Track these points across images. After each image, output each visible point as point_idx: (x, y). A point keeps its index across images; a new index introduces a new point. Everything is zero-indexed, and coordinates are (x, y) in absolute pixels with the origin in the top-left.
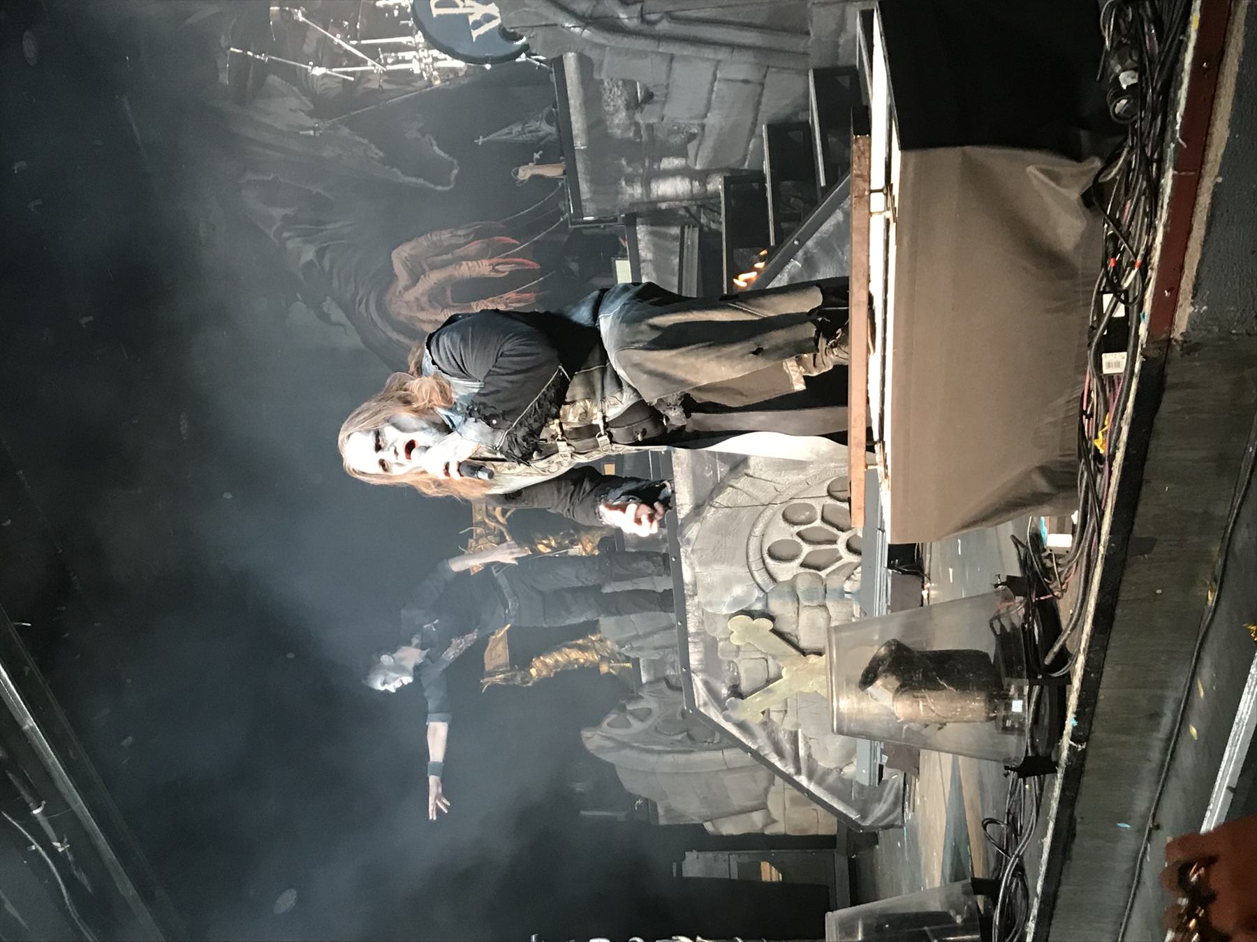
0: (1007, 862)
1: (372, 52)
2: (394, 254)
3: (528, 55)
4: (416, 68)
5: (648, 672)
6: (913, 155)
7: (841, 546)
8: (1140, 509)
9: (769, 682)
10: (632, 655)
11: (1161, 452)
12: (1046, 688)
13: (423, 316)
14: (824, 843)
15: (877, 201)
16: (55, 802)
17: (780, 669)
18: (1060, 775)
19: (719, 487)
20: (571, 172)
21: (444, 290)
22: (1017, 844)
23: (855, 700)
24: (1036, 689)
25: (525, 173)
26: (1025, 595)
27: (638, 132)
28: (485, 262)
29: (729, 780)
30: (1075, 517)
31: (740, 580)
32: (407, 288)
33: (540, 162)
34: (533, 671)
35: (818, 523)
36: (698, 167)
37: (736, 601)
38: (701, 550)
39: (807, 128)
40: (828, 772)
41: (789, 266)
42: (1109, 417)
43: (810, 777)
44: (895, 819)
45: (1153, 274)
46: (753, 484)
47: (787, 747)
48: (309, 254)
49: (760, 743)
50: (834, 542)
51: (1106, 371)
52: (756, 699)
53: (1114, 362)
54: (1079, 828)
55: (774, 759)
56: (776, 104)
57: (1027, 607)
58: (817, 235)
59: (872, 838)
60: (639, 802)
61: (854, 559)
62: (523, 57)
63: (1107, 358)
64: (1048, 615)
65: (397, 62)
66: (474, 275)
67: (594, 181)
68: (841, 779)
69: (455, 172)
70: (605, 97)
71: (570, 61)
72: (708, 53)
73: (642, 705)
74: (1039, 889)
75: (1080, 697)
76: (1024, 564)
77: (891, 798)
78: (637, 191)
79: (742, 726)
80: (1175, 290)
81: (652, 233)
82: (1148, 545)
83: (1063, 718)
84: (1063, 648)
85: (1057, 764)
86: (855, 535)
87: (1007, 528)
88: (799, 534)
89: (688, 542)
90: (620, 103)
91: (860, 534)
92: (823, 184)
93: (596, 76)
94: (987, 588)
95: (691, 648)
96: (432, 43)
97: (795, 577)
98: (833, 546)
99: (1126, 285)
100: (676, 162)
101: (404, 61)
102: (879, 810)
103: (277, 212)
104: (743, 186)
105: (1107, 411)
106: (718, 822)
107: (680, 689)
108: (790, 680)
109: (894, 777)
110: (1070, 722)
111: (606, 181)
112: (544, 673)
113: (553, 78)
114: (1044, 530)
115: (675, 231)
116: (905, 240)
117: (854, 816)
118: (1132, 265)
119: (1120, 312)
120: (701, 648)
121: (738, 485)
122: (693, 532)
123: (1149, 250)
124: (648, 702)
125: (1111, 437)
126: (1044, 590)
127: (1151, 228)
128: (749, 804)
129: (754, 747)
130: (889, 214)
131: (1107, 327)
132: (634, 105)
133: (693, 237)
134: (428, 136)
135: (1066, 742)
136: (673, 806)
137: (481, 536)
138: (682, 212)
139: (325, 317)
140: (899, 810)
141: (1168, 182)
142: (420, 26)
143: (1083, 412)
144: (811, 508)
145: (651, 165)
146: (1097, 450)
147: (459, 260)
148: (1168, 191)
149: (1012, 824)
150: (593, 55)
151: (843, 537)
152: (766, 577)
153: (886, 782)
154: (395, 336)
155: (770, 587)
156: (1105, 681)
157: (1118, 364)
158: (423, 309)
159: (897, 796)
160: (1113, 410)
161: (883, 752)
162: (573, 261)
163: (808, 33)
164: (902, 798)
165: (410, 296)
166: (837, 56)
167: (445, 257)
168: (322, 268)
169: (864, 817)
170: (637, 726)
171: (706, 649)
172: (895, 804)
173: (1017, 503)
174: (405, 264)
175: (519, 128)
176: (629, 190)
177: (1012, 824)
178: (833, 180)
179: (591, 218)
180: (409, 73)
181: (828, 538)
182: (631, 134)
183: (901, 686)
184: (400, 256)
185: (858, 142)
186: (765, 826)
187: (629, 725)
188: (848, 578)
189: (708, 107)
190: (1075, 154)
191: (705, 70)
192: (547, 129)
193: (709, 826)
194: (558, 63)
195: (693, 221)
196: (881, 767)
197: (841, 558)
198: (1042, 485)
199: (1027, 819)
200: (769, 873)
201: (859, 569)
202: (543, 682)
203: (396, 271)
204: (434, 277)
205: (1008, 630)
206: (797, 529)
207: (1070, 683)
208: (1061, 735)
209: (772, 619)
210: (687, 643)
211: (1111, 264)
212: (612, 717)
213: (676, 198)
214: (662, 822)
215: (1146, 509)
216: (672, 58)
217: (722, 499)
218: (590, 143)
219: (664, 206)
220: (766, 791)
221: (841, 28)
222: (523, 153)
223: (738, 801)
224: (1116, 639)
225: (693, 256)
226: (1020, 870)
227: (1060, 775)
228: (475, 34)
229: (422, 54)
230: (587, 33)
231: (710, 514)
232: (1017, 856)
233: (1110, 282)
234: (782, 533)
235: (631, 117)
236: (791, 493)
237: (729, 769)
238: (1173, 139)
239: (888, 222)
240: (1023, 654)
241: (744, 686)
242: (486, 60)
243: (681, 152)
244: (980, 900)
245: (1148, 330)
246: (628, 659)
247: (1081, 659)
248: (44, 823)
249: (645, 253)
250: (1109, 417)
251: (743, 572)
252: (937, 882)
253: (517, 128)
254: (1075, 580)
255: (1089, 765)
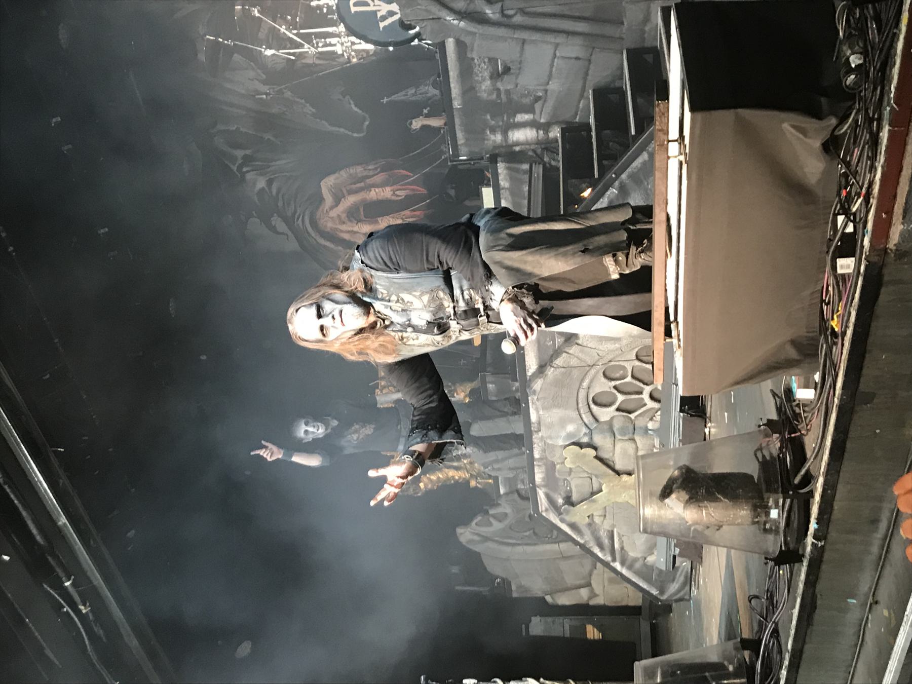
0: (766, 627)
1: (307, 38)
2: (322, 183)
3: (420, 40)
4: (339, 49)
5: (505, 486)
6: (699, 116)
7: (645, 396)
8: (865, 371)
9: (593, 494)
10: (493, 474)
11: (879, 330)
12: (795, 501)
13: (344, 227)
14: (634, 611)
15: (674, 148)
16: (82, 580)
17: (601, 485)
18: (805, 563)
19: (557, 353)
20: (450, 124)
21: (358, 209)
22: (774, 613)
23: (656, 508)
24: (788, 501)
25: (417, 124)
26: (780, 433)
27: (499, 95)
28: (388, 189)
29: (564, 565)
30: (817, 377)
31: (571, 421)
32: (332, 208)
33: (427, 116)
34: (422, 485)
35: (629, 379)
36: (542, 121)
37: (569, 435)
38: (545, 398)
39: (623, 94)
40: (636, 560)
41: (608, 193)
42: (842, 304)
43: (623, 564)
44: (685, 594)
45: (874, 202)
46: (582, 351)
47: (606, 542)
48: (261, 183)
49: (586, 538)
50: (641, 393)
51: (839, 271)
52: (583, 506)
53: (846, 265)
54: (819, 602)
55: (597, 550)
56: (599, 74)
57: (782, 442)
58: (629, 170)
59: (667, 608)
60: (498, 580)
61: (656, 405)
62: (416, 42)
63: (840, 262)
64: (797, 448)
65: (326, 45)
66: (380, 198)
67: (468, 131)
68: (645, 565)
69: (367, 123)
70: (475, 70)
71: (450, 44)
72: (550, 38)
73: (499, 510)
74: (790, 647)
75: (820, 508)
76: (779, 410)
77: (682, 579)
78: (498, 138)
79: (573, 526)
80: (890, 213)
81: (508, 168)
82: (869, 398)
83: (808, 522)
84: (808, 471)
85: (803, 556)
86: (656, 389)
87: (767, 385)
88: (615, 387)
89: (534, 392)
90: (486, 74)
91: (660, 388)
92: (633, 133)
93: (469, 55)
94: (753, 428)
95: (536, 470)
96: (351, 32)
97: (612, 418)
98: (640, 396)
99: (854, 209)
100: (527, 117)
101: (331, 45)
102: (673, 588)
103: (239, 153)
104: (574, 134)
105: (840, 300)
106: (556, 596)
107: (528, 499)
108: (609, 493)
109: (684, 564)
110: (813, 526)
111: (476, 132)
112: (430, 486)
113: (438, 56)
114: (794, 386)
115: (526, 167)
116: (694, 177)
117: (655, 592)
118: (858, 195)
119: (850, 229)
120: (543, 469)
121: (571, 352)
122: (538, 385)
123: (871, 184)
124: (505, 508)
125: (843, 319)
126: (794, 430)
127: (873, 168)
128: (578, 582)
129: (582, 541)
130: (682, 158)
131: (840, 240)
132: (496, 76)
133: (538, 171)
134: (348, 97)
135: (810, 540)
136: (523, 583)
137: (384, 387)
138: (531, 153)
139: (273, 229)
140: (687, 588)
141: (885, 135)
142: (342, 19)
143: (823, 301)
144: (624, 368)
145: (508, 118)
146: (833, 329)
147: (369, 188)
148: (885, 141)
149: (771, 598)
150: (467, 40)
151: (647, 390)
152: (591, 418)
153: (679, 567)
154: (322, 242)
155: (593, 425)
156: (838, 496)
157: (848, 266)
158: (344, 223)
159: (686, 577)
160: (844, 299)
161: (675, 546)
162: (452, 188)
163: (622, 23)
164: (690, 579)
165: (334, 213)
166: (643, 39)
167: (359, 185)
168: (271, 192)
169: (662, 592)
170: (497, 526)
171: (547, 470)
172: (684, 584)
173: (775, 366)
174: (330, 190)
175: (413, 91)
176: (492, 137)
177: (771, 598)
178: (640, 130)
179: (465, 158)
180: (334, 53)
181: (636, 390)
182: (494, 96)
183: (690, 498)
184: (327, 184)
185: (659, 106)
186: (590, 598)
187: (491, 524)
188: (651, 419)
189: (550, 77)
190: (817, 114)
191: (549, 50)
192: (433, 92)
193: (548, 598)
194: (442, 46)
195: (539, 159)
196: (674, 557)
197: (645, 405)
198: (793, 353)
199: (782, 595)
200: (592, 633)
201: (659, 413)
202: (428, 493)
203: (325, 197)
204: (350, 200)
205: (768, 458)
206: (613, 383)
207: (813, 497)
208: (806, 535)
209: (595, 448)
210: (533, 466)
211: (844, 193)
212: (479, 518)
213: (527, 143)
214: (515, 595)
215: (869, 371)
216: (524, 42)
217: (559, 362)
218: (464, 103)
219: (517, 149)
220: (590, 575)
221: (647, 19)
222: (416, 110)
223: (570, 580)
224: (847, 467)
225: (539, 186)
226: (775, 633)
227: (805, 563)
228: (382, 25)
229: (343, 40)
230: (462, 24)
231: (550, 372)
232: (774, 622)
233: (842, 207)
234: (603, 386)
235: (494, 85)
236: (610, 357)
237: (563, 557)
238: (889, 104)
239: (681, 163)
240: (779, 475)
241: (575, 497)
242: (389, 44)
243: (530, 110)
244: (747, 654)
245: (871, 242)
246: (490, 477)
247: (821, 480)
248: (72, 591)
249: (504, 183)
250: (842, 304)
251: (574, 414)
252: (715, 641)
253: (412, 91)
254: (817, 422)
255: (826, 556)
